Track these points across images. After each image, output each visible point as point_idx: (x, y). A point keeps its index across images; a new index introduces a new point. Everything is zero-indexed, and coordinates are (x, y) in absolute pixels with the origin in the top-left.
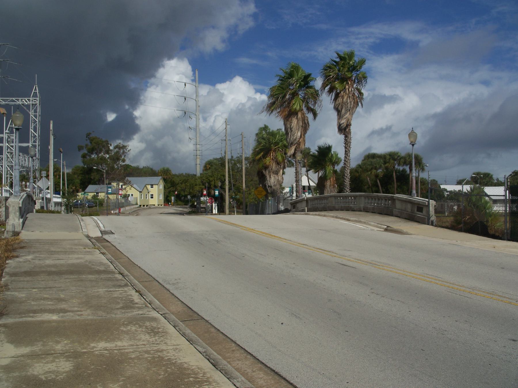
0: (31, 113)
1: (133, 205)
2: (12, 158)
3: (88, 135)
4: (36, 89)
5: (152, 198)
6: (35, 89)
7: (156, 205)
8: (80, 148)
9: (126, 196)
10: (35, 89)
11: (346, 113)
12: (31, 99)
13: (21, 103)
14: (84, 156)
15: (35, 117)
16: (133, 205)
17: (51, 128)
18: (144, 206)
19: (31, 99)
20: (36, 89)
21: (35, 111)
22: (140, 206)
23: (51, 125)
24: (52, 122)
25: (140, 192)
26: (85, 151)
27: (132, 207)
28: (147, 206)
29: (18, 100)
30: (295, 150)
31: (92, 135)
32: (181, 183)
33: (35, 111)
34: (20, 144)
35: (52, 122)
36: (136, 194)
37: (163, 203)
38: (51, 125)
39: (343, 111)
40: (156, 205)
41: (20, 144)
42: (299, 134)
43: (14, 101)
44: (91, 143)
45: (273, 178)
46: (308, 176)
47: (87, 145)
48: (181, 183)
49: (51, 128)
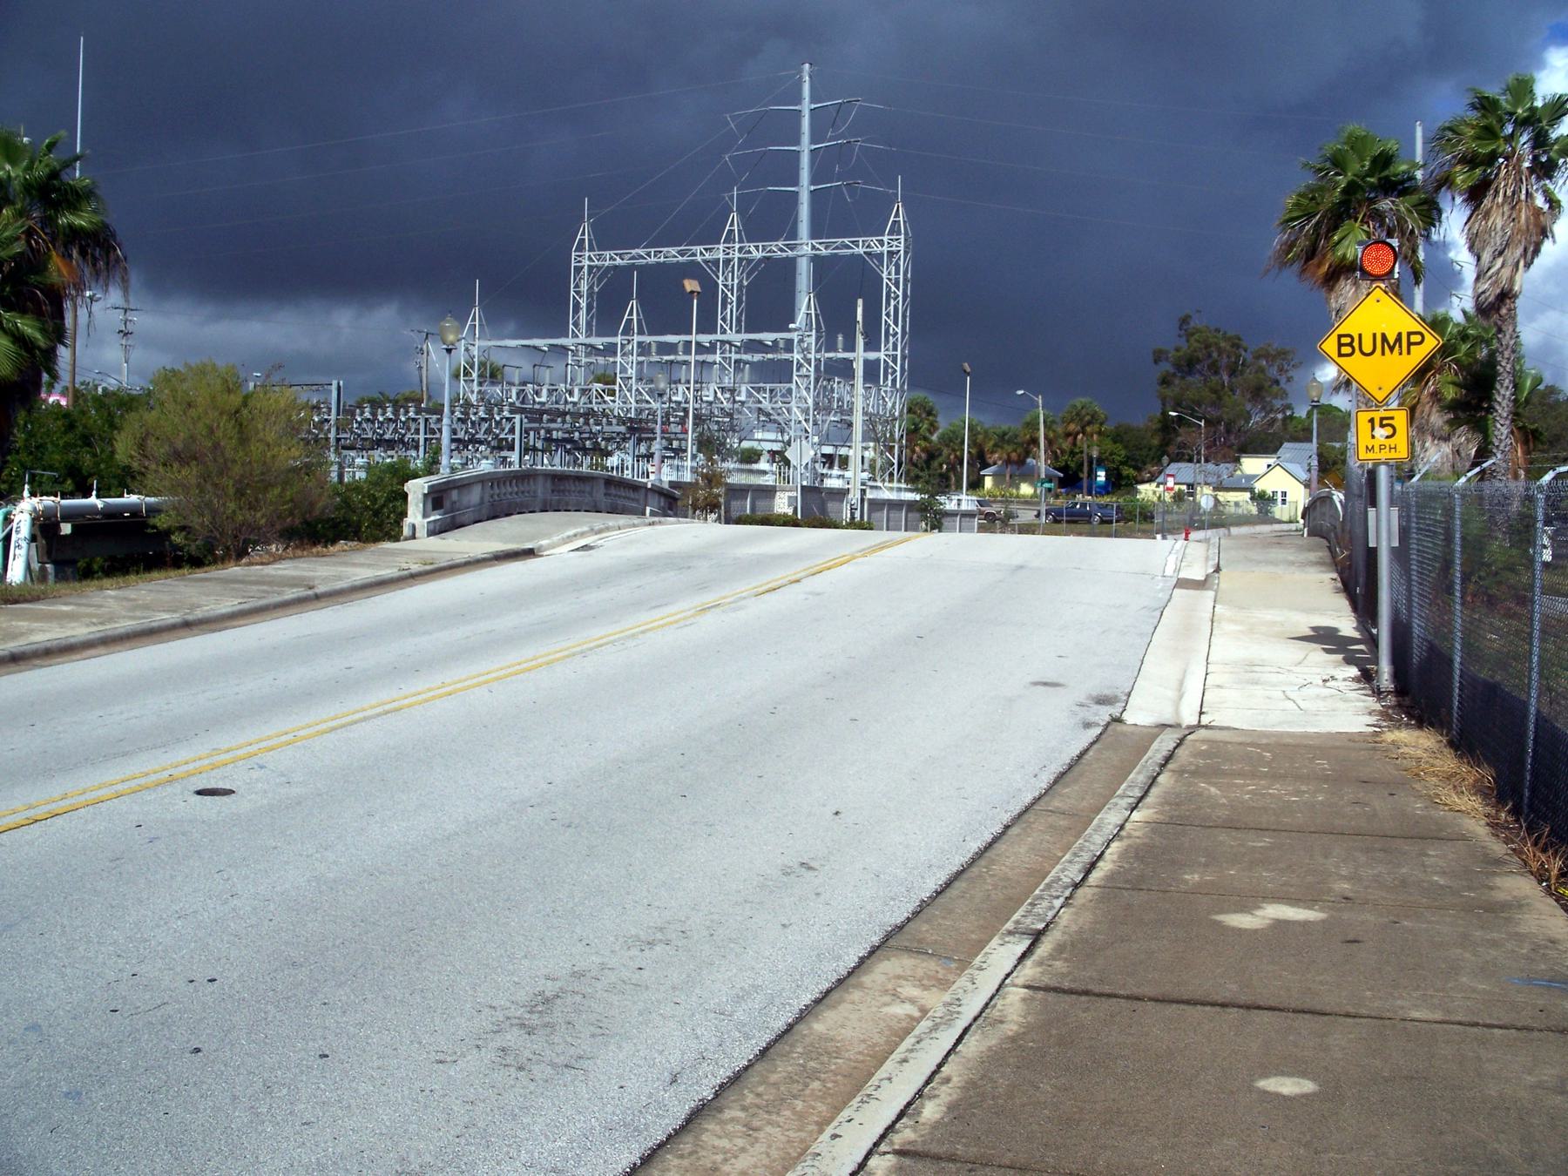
1: (1280, 522)
3: (1185, 321)
4: (899, 214)
6: (897, 215)
10: (897, 215)
12: (885, 239)
13: (861, 250)
16: (1280, 522)
17: (859, 318)
19: (885, 239)
20: (899, 214)
23: (860, 311)
24: (860, 302)
27: (1277, 527)
29: (856, 243)
31: (1195, 323)
35: (860, 302)
38: (860, 311)
43: (848, 247)
45: (1432, 450)
49: (859, 318)
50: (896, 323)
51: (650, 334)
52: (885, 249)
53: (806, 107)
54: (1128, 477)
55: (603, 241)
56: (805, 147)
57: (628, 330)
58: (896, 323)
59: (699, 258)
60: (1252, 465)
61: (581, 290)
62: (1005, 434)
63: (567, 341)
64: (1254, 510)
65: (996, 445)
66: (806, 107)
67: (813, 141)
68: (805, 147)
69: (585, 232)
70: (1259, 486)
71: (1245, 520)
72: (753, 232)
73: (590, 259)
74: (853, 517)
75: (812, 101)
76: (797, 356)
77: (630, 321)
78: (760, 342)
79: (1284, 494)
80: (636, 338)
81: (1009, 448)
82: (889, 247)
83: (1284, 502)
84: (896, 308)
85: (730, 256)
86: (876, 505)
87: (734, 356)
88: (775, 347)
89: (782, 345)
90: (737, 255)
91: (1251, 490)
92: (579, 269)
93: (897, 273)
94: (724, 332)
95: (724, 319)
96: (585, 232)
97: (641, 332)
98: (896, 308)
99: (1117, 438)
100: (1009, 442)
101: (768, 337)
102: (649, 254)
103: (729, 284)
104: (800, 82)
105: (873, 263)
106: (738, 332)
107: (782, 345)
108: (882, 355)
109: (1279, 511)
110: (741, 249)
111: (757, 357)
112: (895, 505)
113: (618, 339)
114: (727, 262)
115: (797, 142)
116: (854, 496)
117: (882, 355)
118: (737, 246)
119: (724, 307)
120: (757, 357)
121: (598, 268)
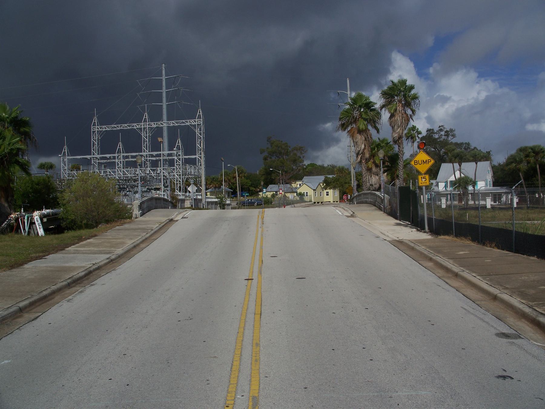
0: (197, 131)
2: (180, 169)
4: (200, 112)
5: (327, 195)
6: (200, 112)
7: (332, 202)
8: (262, 152)
9: (301, 195)
11: (397, 129)
12: (196, 120)
14: (265, 159)
15: (200, 135)
18: (318, 203)
19: (196, 120)
20: (200, 112)
21: (200, 130)
22: (315, 203)
25: (314, 190)
26: (266, 154)
27: (307, 203)
28: (322, 203)
30: (361, 158)
32: (334, 182)
33: (200, 130)
34: (185, 157)
36: (311, 192)
37: (339, 200)
39: (396, 127)
40: (332, 202)
41: (185, 157)
42: (363, 146)
43: (184, 123)
44: (271, 146)
46: (460, 171)
47: (268, 148)
48: (334, 182)
50: (200, 146)
51: (71, 156)
52: (196, 123)
53: (164, 78)
54: (252, 190)
55: (101, 123)
56: (164, 90)
57: (119, 152)
58: (200, 146)
59: (135, 128)
60: (296, 185)
61: (95, 139)
62: (214, 178)
63: (143, 153)
64: (298, 198)
65: (211, 182)
66: (164, 78)
67: (166, 89)
68: (164, 90)
69: (95, 120)
70: (299, 191)
71: (297, 202)
72: (152, 119)
73: (98, 128)
74: (203, 207)
75: (166, 76)
76: (117, 160)
77: (119, 149)
78: (106, 157)
79: (307, 193)
80: (122, 154)
81: (216, 183)
82: (197, 122)
83: (307, 195)
84: (147, 145)
85: (145, 127)
86: (209, 203)
87: (97, 161)
88: (110, 158)
89: (112, 158)
90: (148, 126)
91: (296, 192)
92: (94, 132)
93: (146, 134)
94: (94, 154)
95: (94, 150)
96: (95, 120)
97: (123, 153)
98: (147, 145)
99: (247, 178)
100: (215, 181)
101: (108, 156)
102: (118, 127)
103: (145, 136)
104: (161, 70)
105: (193, 128)
106: (98, 154)
107: (112, 158)
108: (197, 156)
109: (306, 198)
110: (149, 125)
111: (105, 161)
112: (212, 203)
113: (116, 155)
114: (144, 128)
115: (162, 89)
116: (204, 201)
117: (197, 156)
118: (148, 123)
119: (93, 146)
120: (105, 161)
121: (101, 131)
